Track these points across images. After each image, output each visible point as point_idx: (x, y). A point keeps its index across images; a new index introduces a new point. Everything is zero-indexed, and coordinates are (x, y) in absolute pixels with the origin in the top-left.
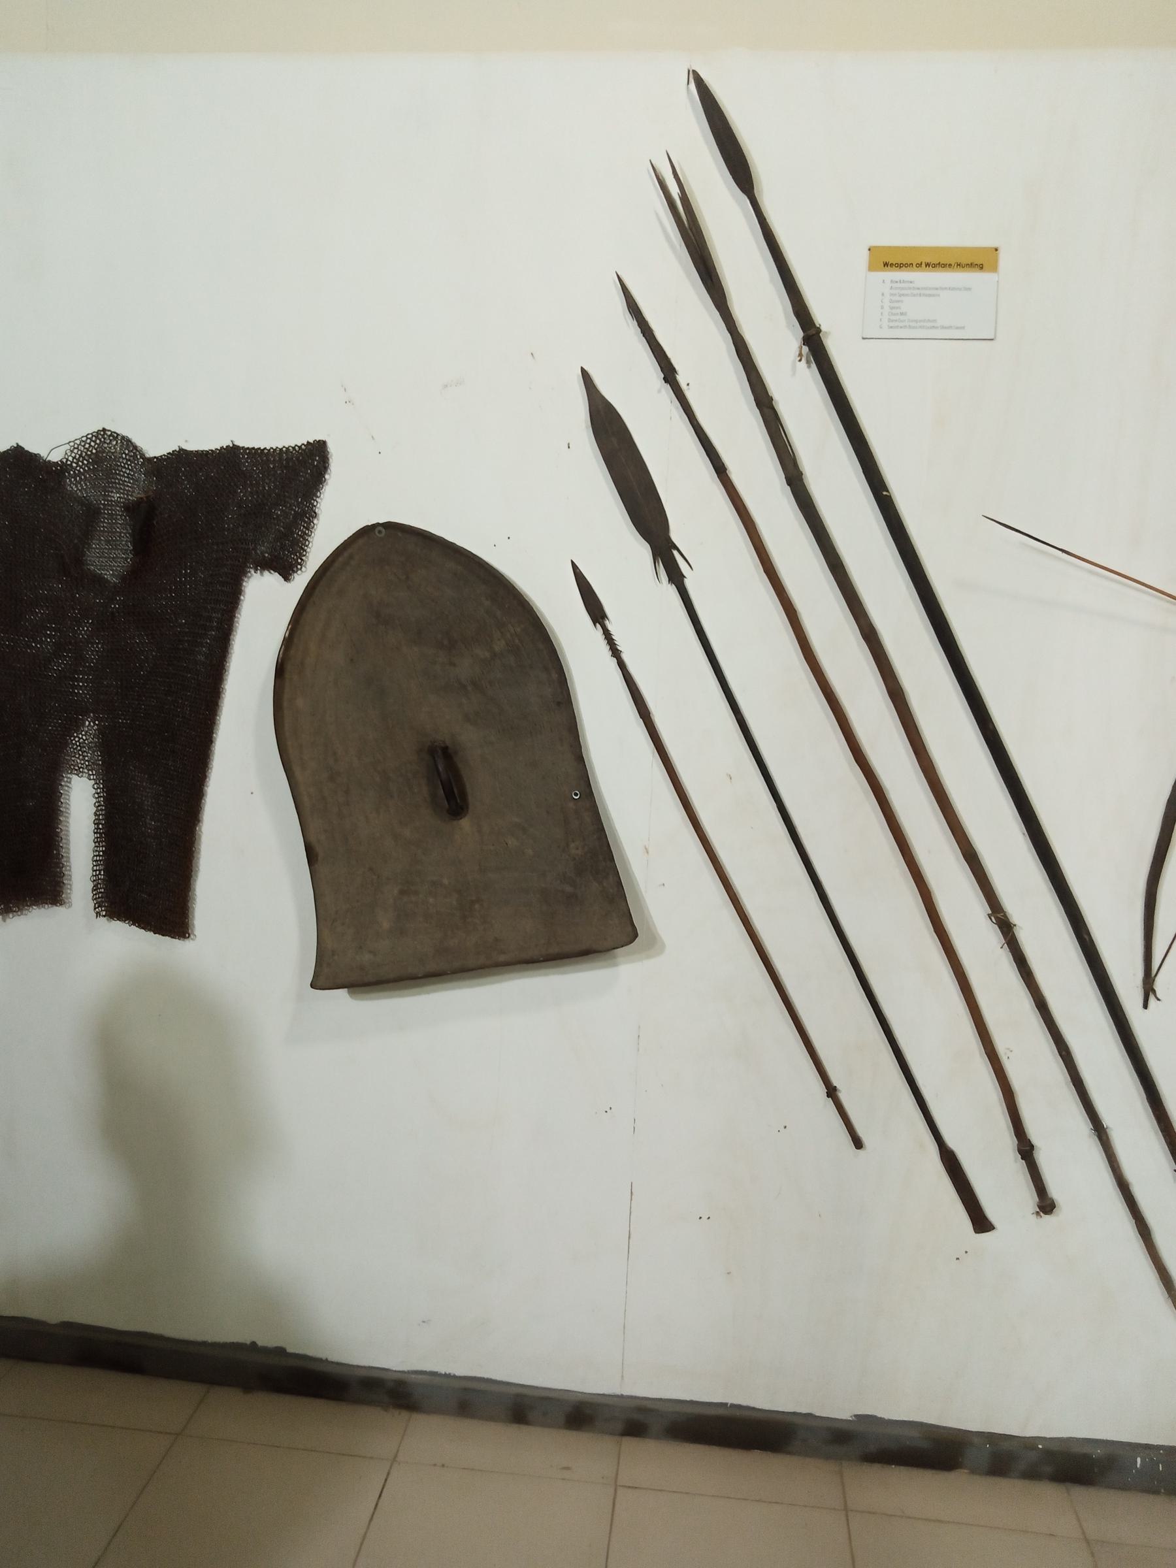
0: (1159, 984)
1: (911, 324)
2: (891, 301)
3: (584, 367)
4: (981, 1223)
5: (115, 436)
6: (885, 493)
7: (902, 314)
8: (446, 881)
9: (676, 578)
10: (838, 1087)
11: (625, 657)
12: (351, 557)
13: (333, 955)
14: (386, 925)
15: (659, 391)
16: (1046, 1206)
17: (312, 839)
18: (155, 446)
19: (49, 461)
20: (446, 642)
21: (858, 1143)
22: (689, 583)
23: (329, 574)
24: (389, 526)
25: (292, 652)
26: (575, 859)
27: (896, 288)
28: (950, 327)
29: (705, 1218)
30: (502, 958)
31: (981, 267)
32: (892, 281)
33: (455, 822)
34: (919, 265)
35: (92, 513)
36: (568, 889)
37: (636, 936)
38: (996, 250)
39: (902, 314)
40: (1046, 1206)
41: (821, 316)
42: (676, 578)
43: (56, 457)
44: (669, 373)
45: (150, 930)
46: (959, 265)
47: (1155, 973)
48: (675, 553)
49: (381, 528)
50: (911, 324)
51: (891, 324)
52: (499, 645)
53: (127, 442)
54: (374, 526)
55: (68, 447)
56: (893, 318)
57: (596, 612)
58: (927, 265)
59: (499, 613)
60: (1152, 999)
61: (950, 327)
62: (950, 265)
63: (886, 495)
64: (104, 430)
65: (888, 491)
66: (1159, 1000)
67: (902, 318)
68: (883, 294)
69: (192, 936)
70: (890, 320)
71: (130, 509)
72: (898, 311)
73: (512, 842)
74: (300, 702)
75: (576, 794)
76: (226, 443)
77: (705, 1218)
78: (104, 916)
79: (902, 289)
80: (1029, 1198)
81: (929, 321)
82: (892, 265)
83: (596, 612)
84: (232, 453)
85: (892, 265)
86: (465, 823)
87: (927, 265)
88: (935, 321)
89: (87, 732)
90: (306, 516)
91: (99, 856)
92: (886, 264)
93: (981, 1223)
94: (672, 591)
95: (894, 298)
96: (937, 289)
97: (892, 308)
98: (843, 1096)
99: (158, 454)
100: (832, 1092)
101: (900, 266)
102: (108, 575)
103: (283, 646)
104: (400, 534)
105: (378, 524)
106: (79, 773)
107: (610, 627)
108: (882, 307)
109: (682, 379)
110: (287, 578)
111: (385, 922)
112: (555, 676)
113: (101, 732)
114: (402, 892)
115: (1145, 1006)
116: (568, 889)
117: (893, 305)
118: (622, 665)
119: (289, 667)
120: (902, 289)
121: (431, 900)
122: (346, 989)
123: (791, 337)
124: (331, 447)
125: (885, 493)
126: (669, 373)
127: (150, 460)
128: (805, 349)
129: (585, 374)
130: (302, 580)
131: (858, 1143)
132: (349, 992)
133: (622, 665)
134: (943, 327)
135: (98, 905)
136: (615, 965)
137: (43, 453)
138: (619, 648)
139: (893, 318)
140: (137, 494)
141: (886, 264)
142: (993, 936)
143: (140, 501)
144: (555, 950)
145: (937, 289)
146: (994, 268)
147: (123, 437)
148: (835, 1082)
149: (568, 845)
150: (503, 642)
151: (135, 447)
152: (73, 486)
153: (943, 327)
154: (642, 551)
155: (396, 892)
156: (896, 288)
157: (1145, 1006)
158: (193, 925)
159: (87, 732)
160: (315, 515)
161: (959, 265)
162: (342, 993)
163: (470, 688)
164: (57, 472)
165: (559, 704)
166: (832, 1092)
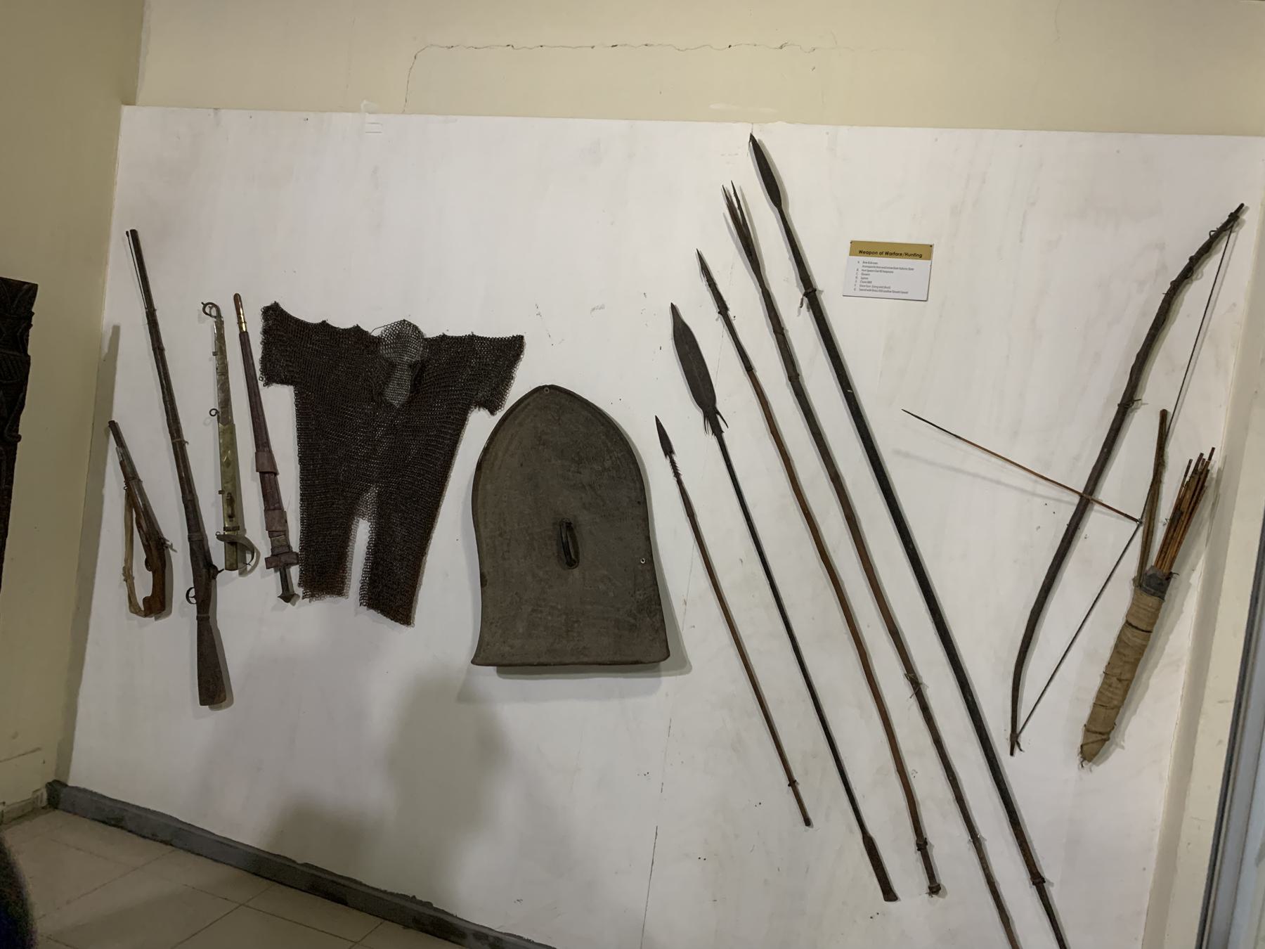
0: (1023, 739)
1: (874, 289)
2: (863, 274)
3: (674, 304)
4: (889, 894)
5: (410, 324)
6: (849, 391)
7: (869, 282)
8: (559, 607)
9: (718, 432)
10: (797, 781)
11: (683, 478)
12: (529, 404)
13: (488, 645)
14: (521, 630)
15: (717, 320)
16: (935, 889)
17: (485, 571)
18: (430, 331)
19: (373, 336)
20: (577, 459)
21: (808, 822)
22: (725, 435)
23: (514, 412)
24: (552, 387)
25: (487, 457)
26: (638, 602)
27: (866, 267)
28: (898, 292)
29: (702, 859)
30: (586, 659)
31: (920, 256)
32: (864, 262)
33: (570, 570)
34: (881, 253)
35: (393, 366)
36: (633, 621)
37: (669, 656)
38: (931, 246)
39: (869, 282)
40: (935, 889)
41: (819, 281)
42: (718, 432)
43: (376, 334)
44: (723, 309)
45: (389, 617)
46: (906, 254)
47: (1020, 728)
48: (718, 417)
49: (547, 388)
50: (874, 289)
51: (862, 288)
52: (608, 464)
53: (415, 328)
54: (544, 387)
55: (383, 328)
56: (862, 284)
57: (668, 449)
58: (887, 253)
59: (609, 444)
60: (1017, 750)
61: (898, 292)
62: (901, 254)
63: (849, 393)
64: (404, 321)
65: (852, 390)
66: (1021, 750)
67: (869, 284)
68: (857, 270)
69: (412, 625)
70: (861, 286)
71: (412, 366)
72: (866, 280)
73: (602, 587)
74: (489, 487)
75: (643, 561)
76: (468, 333)
77: (702, 859)
78: (365, 606)
79: (870, 267)
80: (925, 883)
81: (885, 287)
82: (864, 253)
83: (668, 449)
84: (472, 338)
85: (864, 253)
86: (576, 572)
87: (887, 253)
88: (889, 287)
89: (371, 496)
90: (506, 378)
91: (367, 568)
92: (860, 252)
93: (889, 894)
94: (713, 440)
95: (865, 272)
96: (892, 268)
97: (862, 278)
98: (800, 788)
99: (431, 337)
100: (792, 783)
101: (869, 253)
102: (395, 403)
103: (1167, 430)
104: (558, 393)
105: (546, 386)
106: (363, 516)
107: (675, 458)
108: (856, 277)
109: (731, 313)
110: (492, 413)
111: (521, 628)
112: (638, 485)
113: (379, 495)
114: (533, 611)
115: (1012, 754)
116: (633, 621)
117: (863, 276)
118: (680, 482)
119: (485, 465)
120: (870, 267)
121: (550, 618)
122: (495, 668)
123: (797, 293)
124: (526, 340)
125: (849, 391)
126: (723, 309)
127: (426, 339)
128: (806, 300)
129: (673, 307)
130: (500, 414)
131: (808, 822)
132: (498, 672)
133: (680, 482)
134: (894, 292)
135: (362, 597)
136: (660, 676)
137: (370, 331)
138: (679, 472)
139: (862, 284)
140: (418, 358)
141: (860, 252)
142: (906, 689)
143: (416, 363)
144: (618, 658)
145: (892, 268)
146: (929, 257)
147: (414, 326)
148: (796, 777)
149: (635, 592)
150: (610, 461)
151: (419, 332)
152: (384, 351)
153: (894, 292)
154: (697, 415)
155: (530, 610)
156: (866, 267)
157: (1012, 754)
158: (414, 618)
159: (371, 496)
160: (512, 378)
161: (906, 254)
162: (492, 669)
163: (587, 488)
164: (377, 341)
165: (639, 503)
166: (792, 783)
